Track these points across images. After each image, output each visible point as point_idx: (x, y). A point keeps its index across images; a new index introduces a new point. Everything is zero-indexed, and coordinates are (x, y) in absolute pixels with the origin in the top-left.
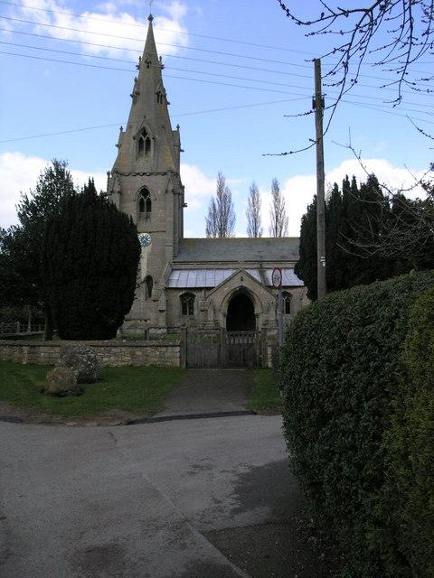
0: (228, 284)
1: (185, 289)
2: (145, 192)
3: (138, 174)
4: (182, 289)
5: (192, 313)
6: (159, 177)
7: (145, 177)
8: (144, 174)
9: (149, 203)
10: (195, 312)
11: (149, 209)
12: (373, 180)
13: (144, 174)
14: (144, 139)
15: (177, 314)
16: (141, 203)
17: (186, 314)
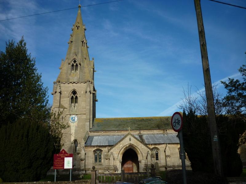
0: (121, 143)
1: (97, 146)
2: (74, 92)
3: (71, 83)
4: (94, 146)
5: (100, 161)
6: (82, 84)
7: (74, 84)
8: (74, 82)
9: (76, 98)
10: (102, 161)
11: (76, 102)
13: (74, 82)
14: (75, 64)
15: (92, 162)
16: (72, 98)
17: (97, 162)
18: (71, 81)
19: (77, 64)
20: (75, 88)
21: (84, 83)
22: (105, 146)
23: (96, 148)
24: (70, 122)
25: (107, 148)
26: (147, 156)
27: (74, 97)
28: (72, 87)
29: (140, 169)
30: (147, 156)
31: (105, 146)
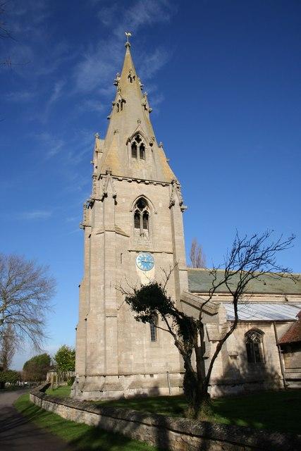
2: (142, 203)
7: (142, 185)
8: (143, 181)
13: (143, 181)
16: (137, 215)
18: (135, 177)
19: (142, 144)
20: (144, 194)
21: (155, 183)
22: (267, 323)
23: (250, 327)
24: (138, 270)
25: (272, 326)
27: (142, 213)
28: (137, 190)
31: (267, 323)
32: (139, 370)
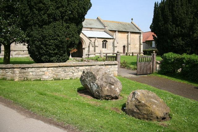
12: (84, 49)
26: (89, 45)
29: (83, 54)
30: (89, 45)
32: (19, 50)
